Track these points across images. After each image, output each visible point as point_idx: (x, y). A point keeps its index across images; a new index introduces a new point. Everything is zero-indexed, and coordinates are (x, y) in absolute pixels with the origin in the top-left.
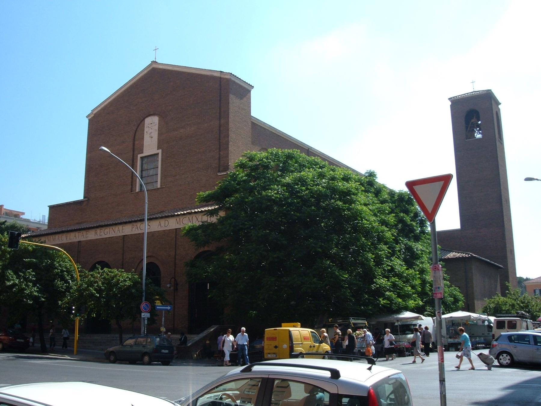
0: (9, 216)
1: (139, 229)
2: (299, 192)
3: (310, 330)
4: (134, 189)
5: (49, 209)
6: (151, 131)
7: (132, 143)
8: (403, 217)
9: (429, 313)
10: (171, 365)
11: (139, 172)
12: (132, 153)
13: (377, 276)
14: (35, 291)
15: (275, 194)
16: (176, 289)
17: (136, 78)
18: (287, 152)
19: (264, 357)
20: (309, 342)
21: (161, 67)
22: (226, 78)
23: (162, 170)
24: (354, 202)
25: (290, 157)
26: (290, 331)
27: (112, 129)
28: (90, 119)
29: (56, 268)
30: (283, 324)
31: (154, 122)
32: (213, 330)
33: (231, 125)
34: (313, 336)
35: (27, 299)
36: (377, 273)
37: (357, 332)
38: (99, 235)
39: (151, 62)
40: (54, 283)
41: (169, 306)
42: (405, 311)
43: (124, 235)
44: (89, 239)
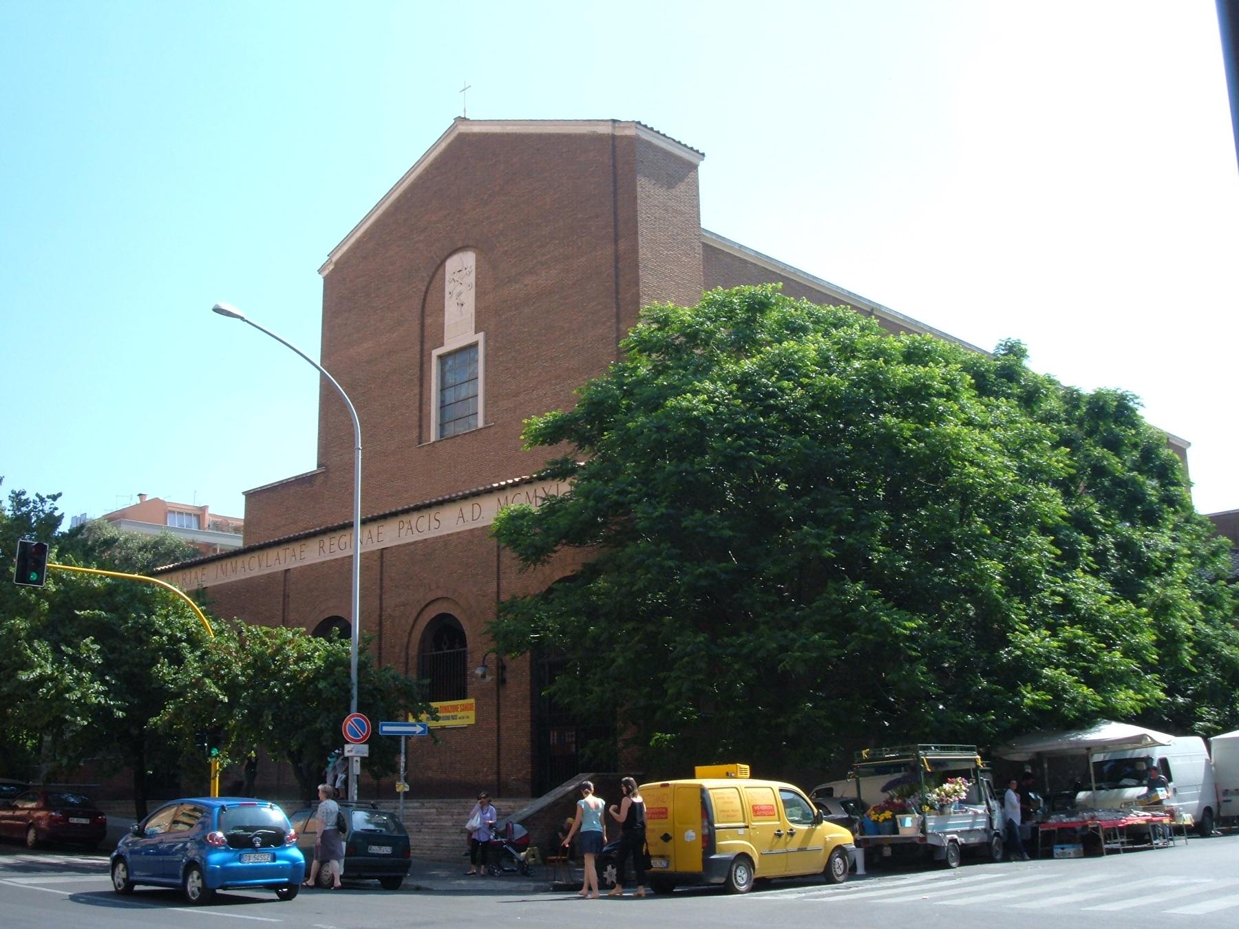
0: (222, 531)
1: (414, 529)
2: (773, 395)
3: (777, 785)
5: (247, 500)
6: (459, 288)
7: (418, 322)
8: (1103, 458)
9: (1209, 725)
10: (418, 890)
12: (418, 348)
13: (1017, 623)
14: (95, 692)
15: (705, 403)
16: (501, 681)
17: (423, 164)
18: (747, 293)
20: (776, 820)
21: (476, 129)
22: (626, 136)
23: (486, 384)
24: (940, 418)
25: (759, 306)
26: (703, 790)
29: (156, 633)
30: (698, 769)
33: (644, 253)
34: (787, 804)
35: (74, 715)
36: (1016, 615)
37: (947, 786)
38: (327, 552)
40: (152, 672)
42: (1105, 723)
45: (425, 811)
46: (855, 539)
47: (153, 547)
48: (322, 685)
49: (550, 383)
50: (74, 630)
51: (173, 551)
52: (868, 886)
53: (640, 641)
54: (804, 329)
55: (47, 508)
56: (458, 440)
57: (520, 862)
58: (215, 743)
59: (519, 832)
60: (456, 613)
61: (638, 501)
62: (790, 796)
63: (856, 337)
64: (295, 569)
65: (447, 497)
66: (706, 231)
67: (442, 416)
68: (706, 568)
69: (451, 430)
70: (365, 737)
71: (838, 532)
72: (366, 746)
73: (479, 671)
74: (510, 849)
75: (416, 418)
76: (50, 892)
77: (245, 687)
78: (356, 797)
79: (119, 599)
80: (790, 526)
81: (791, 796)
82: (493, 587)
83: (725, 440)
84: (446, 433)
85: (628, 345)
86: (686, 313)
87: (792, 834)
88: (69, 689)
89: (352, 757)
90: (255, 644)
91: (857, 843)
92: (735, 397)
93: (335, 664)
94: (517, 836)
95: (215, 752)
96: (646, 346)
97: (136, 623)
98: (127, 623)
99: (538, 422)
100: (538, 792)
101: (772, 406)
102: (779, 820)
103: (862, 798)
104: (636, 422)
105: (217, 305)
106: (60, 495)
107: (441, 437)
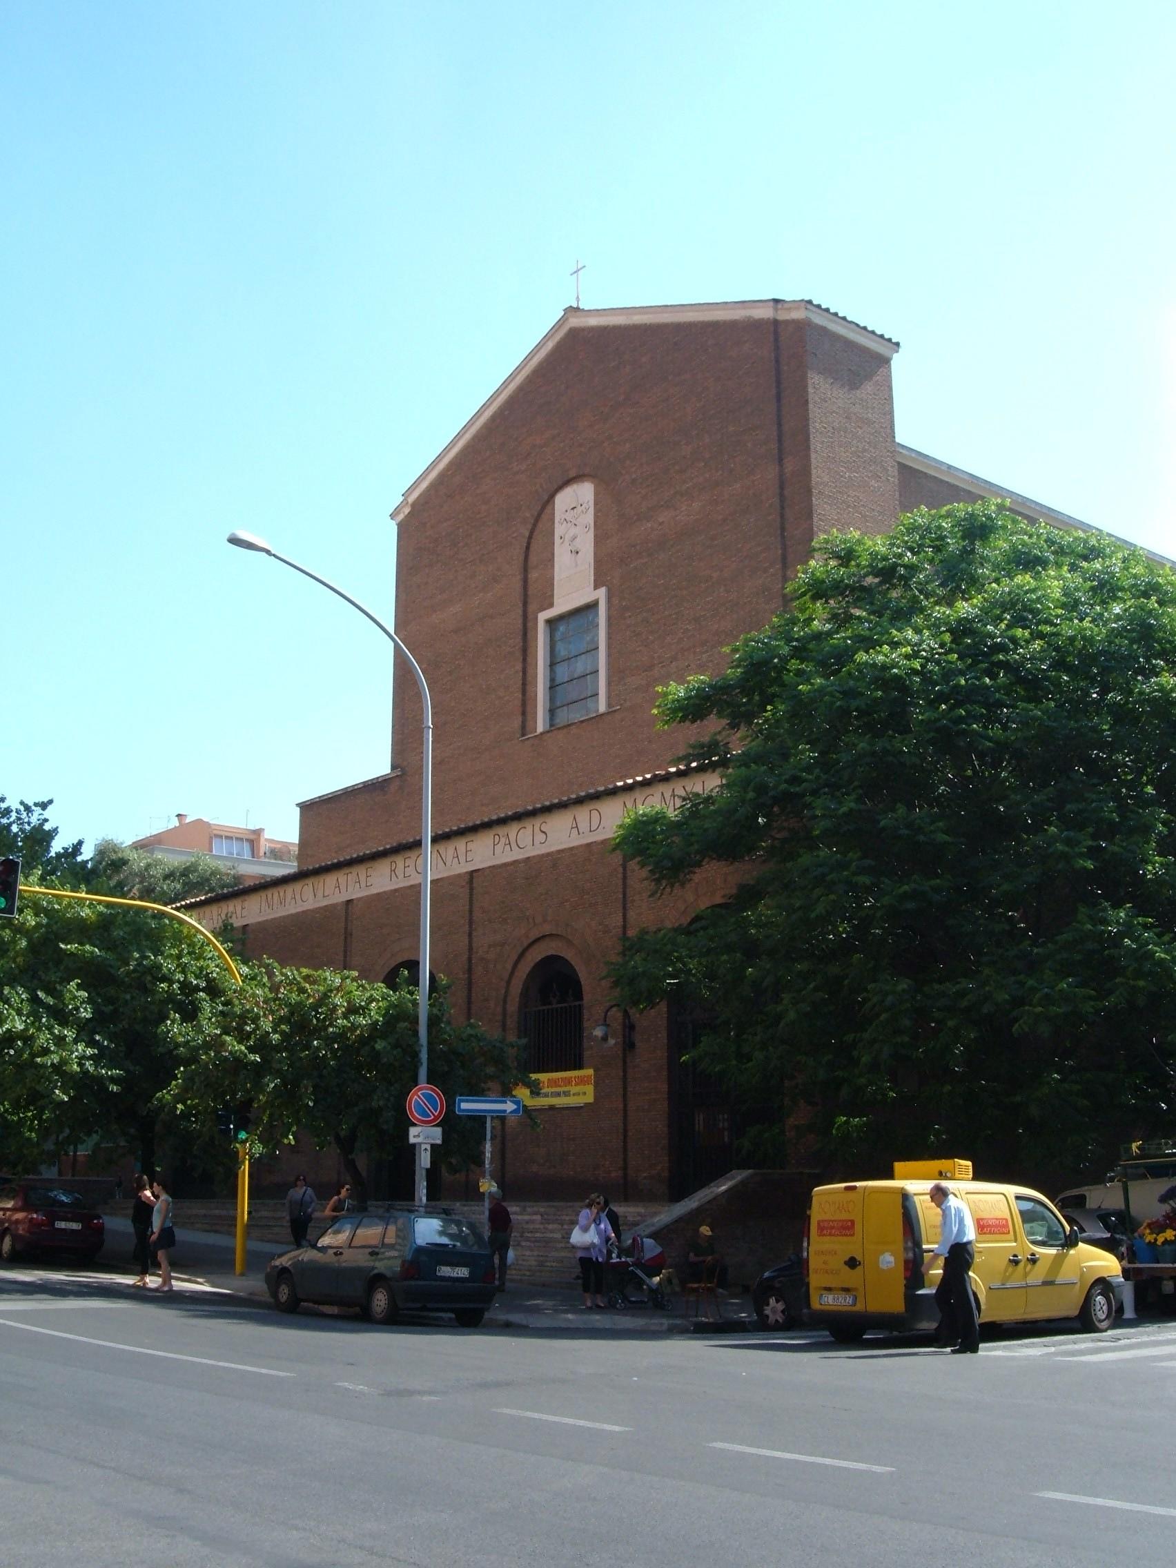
0: (282, 860)
2: (1001, 648)
3: (1012, 1190)
4: (529, 724)
10: (508, 1328)
11: (544, 669)
12: (520, 612)
15: (907, 657)
19: (808, 1305)
21: (593, 322)
22: (793, 321)
23: (609, 655)
26: (905, 1196)
27: (461, 544)
28: (401, 521)
29: (164, 979)
30: (899, 1166)
31: (580, 502)
32: (726, 1191)
33: (819, 474)
34: (1027, 1217)
39: (563, 313)
41: (511, 1101)
43: (472, 871)
44: (375, 892)
45: (526, 1217)
46: (1122, 847)
47: (183, 875)
48: (380, 1045)
49: (695, 653)
50: (59, 974)
51: (208, 880)
52: (1145, 1339)
53: (816, 989)
54: (1044, 563)
55: (34, 820)
56: (574, 730)
57: (651, 1289)
58: (243, 1124)
59: (651, 1248)
60: (568, 955)
61: (814, 793)
62: (1028, 1206)
63: (1117, 570)
64: (359, 899)
65: (556, 801)
66: (903, 446)
67: (552, 699)
68: (913, 885)
69: (563, 717)
70: (436, 1118)
71: (1095, 837)
72: (439, 1130)
73: (598, 1032)
74: (639, 1272)
75: (518, 703)
76: (11, 1327)
77: (277, 1048)
78: (424, 1199)
79: (118, 933)
80: (1028, 829)
81: (1029, 1205)
82: (617, 920)
83: (938, 708)
84: (558, 721)
85: (795, 591)
86: (879, 544)
87: (1033, 1260)
88: (45, 1052)
89: (420, 1144)
90: (291, 991)
91: (1126, 1273)
92: (951, 651)
93: (399, 1018)
94: (648, 1255)
95: (243, 1135)
96: (819, 590)
97: (140, 964)
98: (128, 965)
99: (678, 691)
100: (677, 1195)
101: (1001, 662)
102: (1016, 1241)
103: (1131, 1210)
104: (812, 684)
105: (233, 534)
106: (51, 802)
107: (551, 725)
